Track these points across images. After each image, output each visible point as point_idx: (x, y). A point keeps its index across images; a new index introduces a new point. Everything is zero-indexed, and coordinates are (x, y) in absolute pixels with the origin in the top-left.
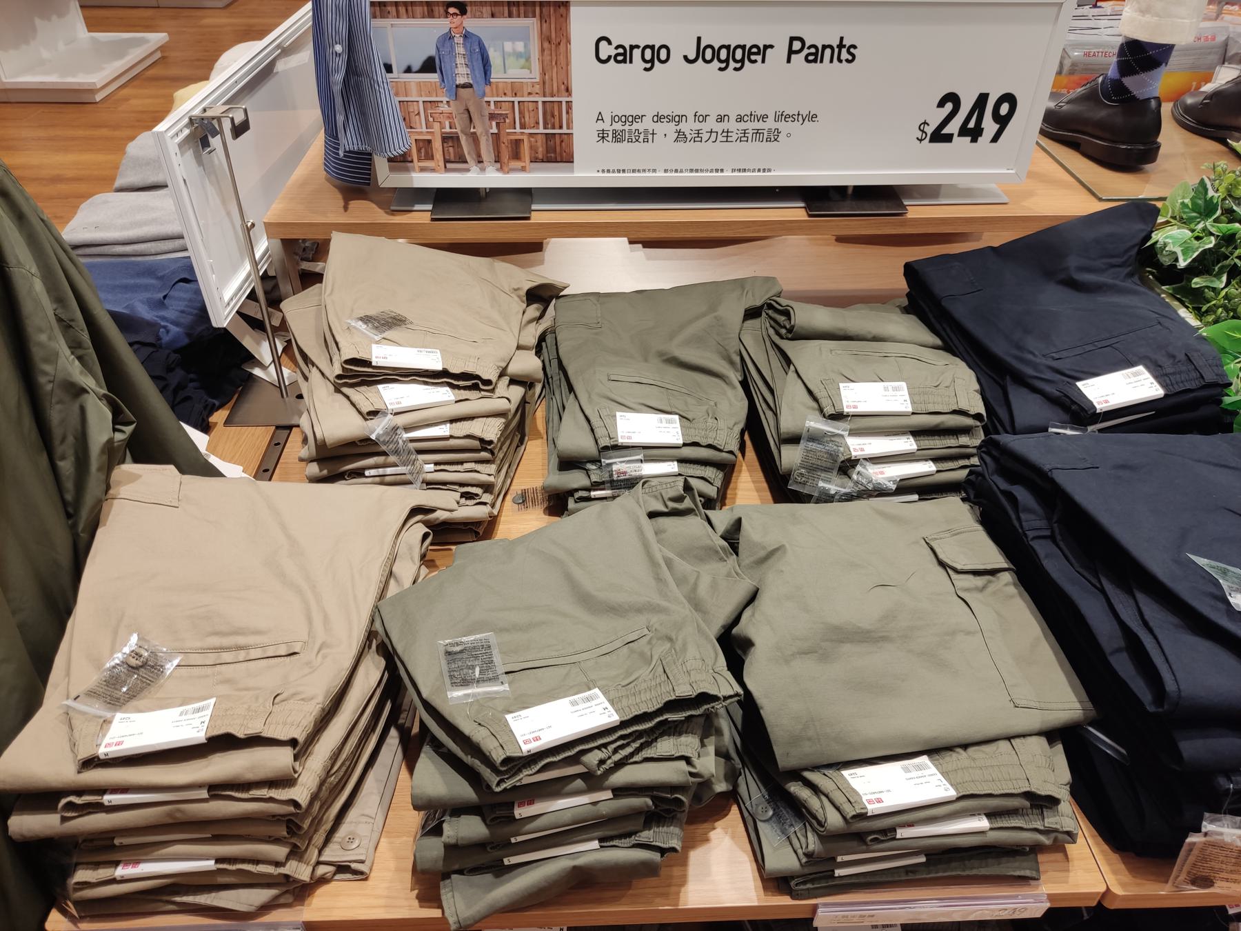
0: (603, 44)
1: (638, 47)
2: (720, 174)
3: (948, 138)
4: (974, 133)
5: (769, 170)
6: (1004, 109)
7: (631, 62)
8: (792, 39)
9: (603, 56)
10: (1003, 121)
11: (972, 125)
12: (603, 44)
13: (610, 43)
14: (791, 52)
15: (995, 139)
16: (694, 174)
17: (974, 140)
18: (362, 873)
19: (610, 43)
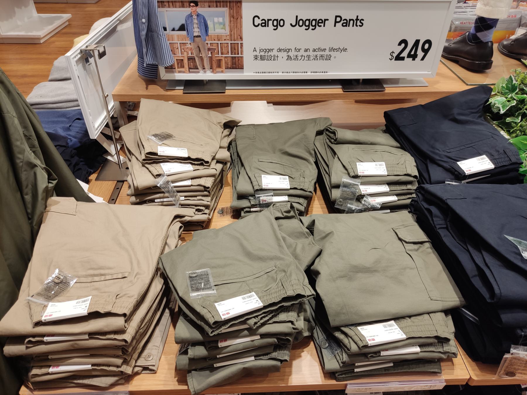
0: (256, 19)
1: (271, 20)
2: (306, 74)
3: (403, 59)
4: (414, 57)
5: (327, 72)
6: (427, 46)
7: (268, 26)
8: (336, 17)
9: (256, 24)
10: (426, 52)
11: (413, 53)
12: (256, 19)
13: (259, 18)
14: (336, 22)
15: (423, 59)
16: (295, 74)
17: (414, 59)
18: (154, 370)
19: (259, 18)
